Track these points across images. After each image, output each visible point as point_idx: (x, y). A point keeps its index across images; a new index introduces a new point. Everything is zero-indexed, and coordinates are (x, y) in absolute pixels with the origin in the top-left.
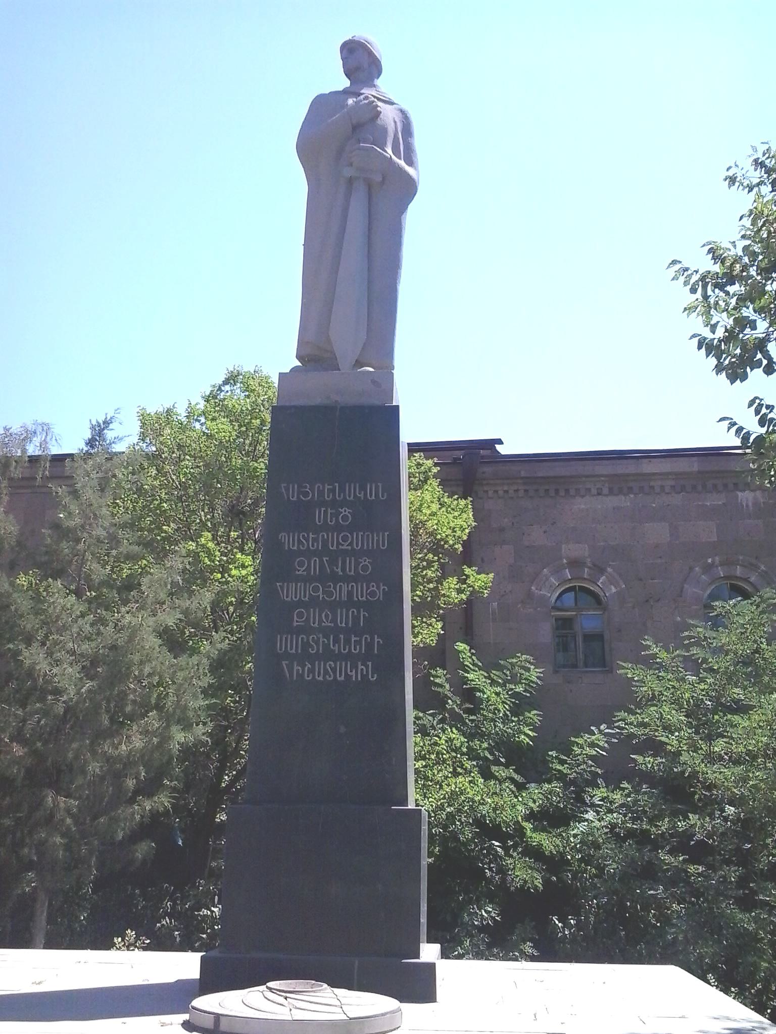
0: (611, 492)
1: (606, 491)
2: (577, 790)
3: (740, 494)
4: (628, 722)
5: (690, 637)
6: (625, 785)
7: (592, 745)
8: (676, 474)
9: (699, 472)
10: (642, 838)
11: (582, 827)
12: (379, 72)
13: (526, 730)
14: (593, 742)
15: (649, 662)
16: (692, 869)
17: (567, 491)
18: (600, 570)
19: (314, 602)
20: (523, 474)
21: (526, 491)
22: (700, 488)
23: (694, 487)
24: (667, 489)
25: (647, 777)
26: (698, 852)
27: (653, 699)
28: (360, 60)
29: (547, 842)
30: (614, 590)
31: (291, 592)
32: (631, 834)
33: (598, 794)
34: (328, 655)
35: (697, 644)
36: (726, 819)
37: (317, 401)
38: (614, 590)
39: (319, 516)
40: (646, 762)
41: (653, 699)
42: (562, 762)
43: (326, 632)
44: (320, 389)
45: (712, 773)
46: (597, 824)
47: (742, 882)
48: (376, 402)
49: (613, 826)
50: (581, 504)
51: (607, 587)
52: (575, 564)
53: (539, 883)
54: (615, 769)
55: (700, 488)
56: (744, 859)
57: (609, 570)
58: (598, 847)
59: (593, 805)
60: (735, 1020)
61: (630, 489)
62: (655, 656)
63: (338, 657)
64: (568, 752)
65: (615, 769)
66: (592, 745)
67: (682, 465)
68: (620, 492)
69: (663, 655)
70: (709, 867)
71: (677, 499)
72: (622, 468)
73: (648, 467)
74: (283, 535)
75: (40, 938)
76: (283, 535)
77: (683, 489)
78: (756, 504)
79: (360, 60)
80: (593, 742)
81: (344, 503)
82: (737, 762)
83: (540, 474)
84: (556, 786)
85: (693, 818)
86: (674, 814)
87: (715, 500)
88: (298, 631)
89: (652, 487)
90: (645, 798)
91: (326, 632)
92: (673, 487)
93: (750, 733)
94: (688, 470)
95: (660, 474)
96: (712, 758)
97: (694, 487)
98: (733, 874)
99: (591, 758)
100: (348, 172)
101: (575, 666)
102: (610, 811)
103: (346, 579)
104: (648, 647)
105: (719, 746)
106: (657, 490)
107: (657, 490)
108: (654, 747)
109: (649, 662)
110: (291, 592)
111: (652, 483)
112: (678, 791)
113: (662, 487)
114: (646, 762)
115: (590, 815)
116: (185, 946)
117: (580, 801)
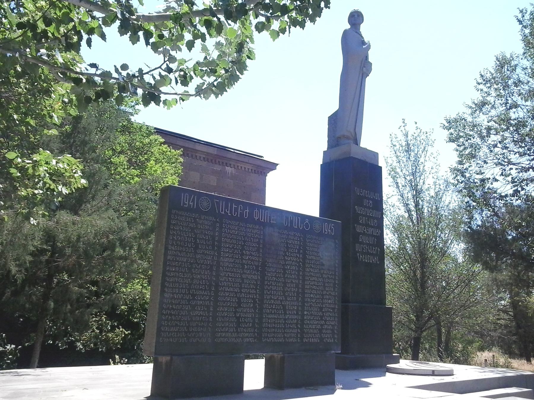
3: (227, 168)
8: (207, 153)
9: (215, 155)
22: (213, 161)
24: (202, 159)
44: (338, 153)
48: (372, 162)
55: (213, 161)
60: (355, 93)
67: (211, 150)
71: (204, 164)
72: (190, 145)
73: (198, 147)
75: (36, 360)
78: (232, 173)
87: (217, 168)
89: (196, 156)
94: (213, 153)
95: (202, 151)
106: (198, 158)
111: (197, 154)
116: (130, 354)
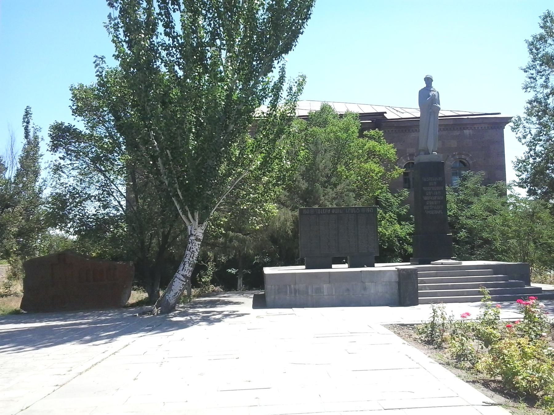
17: (409, 130)
24: (442, 130)
28: (428, 80)
34: (434, 209)
77: (447, 129)
79: (428, 80)
87: (456, 133)
100: (431, 110)
110: (426, 198)
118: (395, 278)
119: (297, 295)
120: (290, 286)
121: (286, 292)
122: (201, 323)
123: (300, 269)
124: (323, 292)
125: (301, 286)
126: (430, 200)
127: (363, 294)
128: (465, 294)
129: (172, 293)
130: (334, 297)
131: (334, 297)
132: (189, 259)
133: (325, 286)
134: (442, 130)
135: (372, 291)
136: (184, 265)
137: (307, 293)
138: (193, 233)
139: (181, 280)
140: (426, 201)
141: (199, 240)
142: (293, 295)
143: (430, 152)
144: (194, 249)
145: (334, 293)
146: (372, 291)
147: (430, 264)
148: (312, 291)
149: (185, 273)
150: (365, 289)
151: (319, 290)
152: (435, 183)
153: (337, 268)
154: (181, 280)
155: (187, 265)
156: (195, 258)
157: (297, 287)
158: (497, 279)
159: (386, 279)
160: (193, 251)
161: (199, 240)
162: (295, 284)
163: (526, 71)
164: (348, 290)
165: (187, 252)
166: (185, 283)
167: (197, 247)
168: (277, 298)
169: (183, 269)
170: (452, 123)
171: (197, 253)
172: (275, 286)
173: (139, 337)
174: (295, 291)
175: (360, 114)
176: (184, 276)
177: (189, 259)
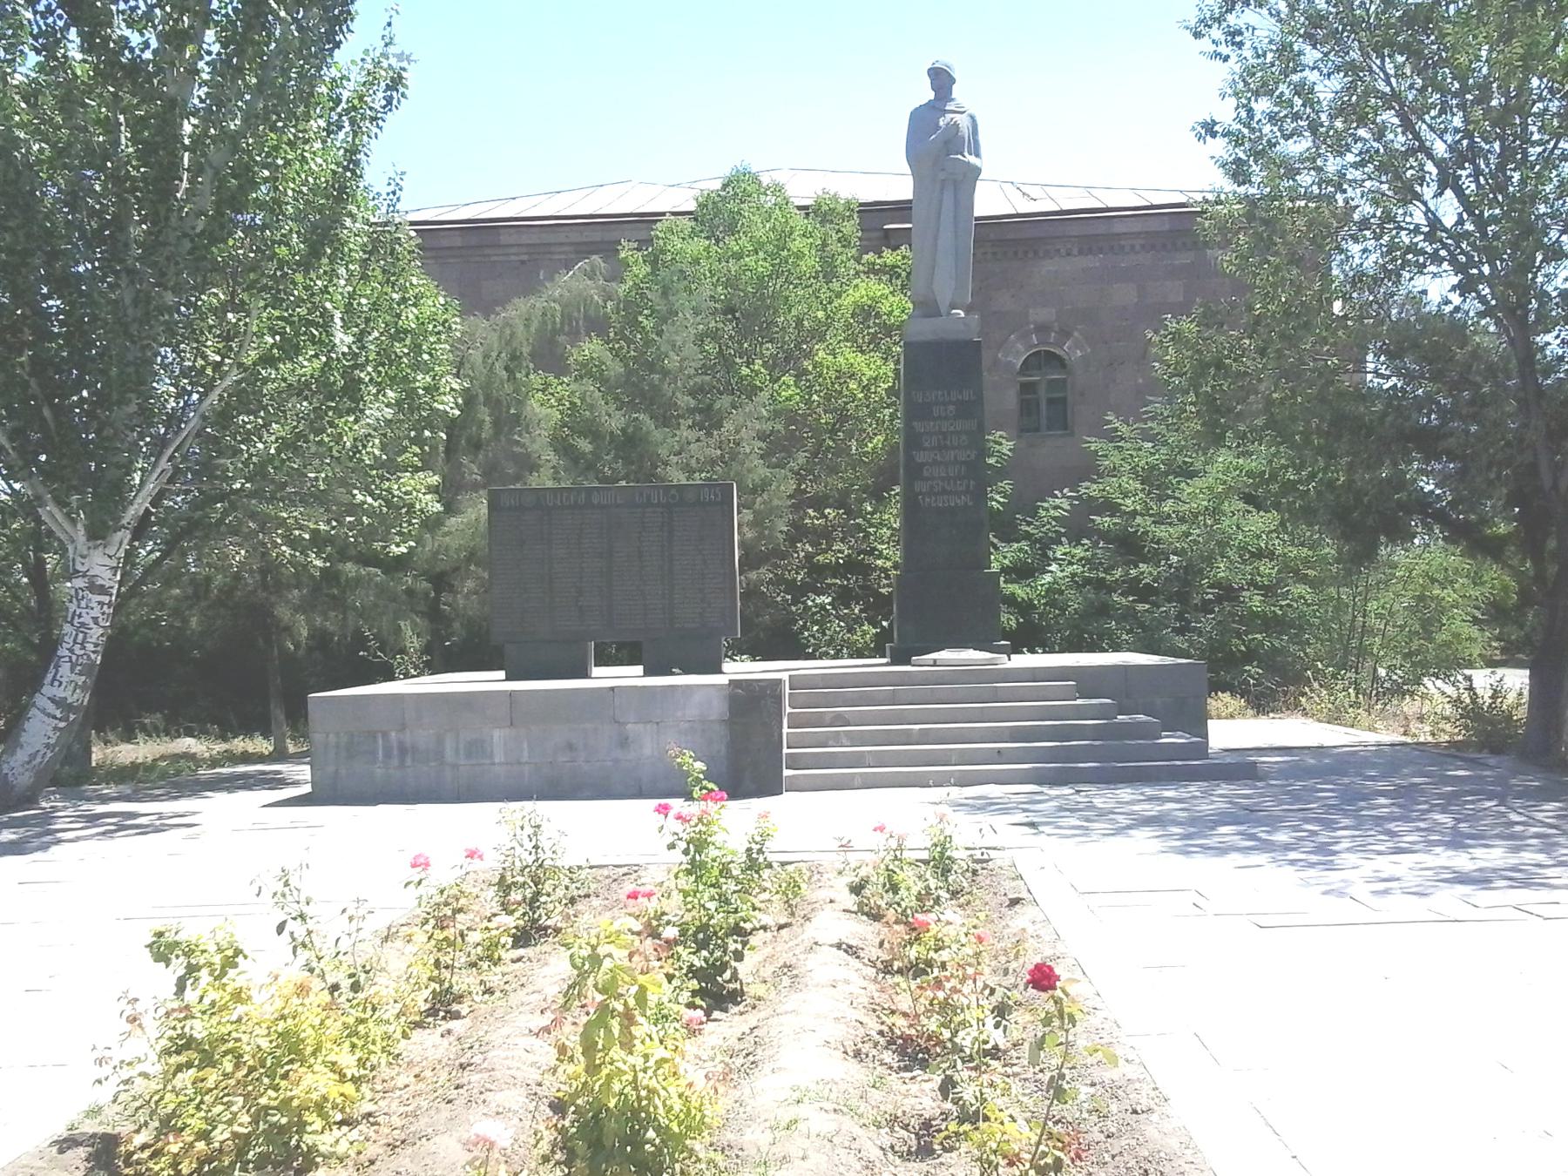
0: (1081, 252)
1: (1075, 251)
2: (1043, 547)
4: (1091, 489)
5: (1146, 412)
6: (1085, 541)
7: (1056, 508)
10: (1100, 584)
11: (1048, 578)
12: (953, 81)
13: (997, 497)
14: (1059, 504)
15: (1112, 436)
16: (1140, 607)
17: (1036, 253)
18: (1065, 334)
19: (935, 463)
20: (992, 236)
21: (994, 254)
23: (1164, 246)
24: (1138, 248)
25: (1105, 535)
26: (1144, 593)
27: (1114, 472)
28: (941, 79)
29: (1019, 591)
30: (1079, 353)
31: (920, 457)
32: (1088, 581)
33: (1059, 552)
34: (944, 492)
35: (1153, 419)
36: (1170, 566)
37: (930, 337)
38: (1079, 353)
39: (936, 411)
40: (1105, 522)
41: (1114, 472)
42: (1029, 524)
43: (943, 479)
45: (1161, 532)
46: (1060, 574)
47: (1180, 617)
49: (1074, 575)
50: (1048, 266)
51: (1072, 351)
52: (1042, 329)
53: (1013, 624)
54: (1076, 528)
56: (1182, 598)
57: (1076, 334)
58: (1061, 592)
59: (1055, 559)
61: (1101, 250)
62: (1116, 430)
63: (950, 493)
64: (1034, 514)
65: (1076, 528)
66: (1056, 508)
67: (1154, 226)
68: (1090, 251)
69: (1124, 429)
70: (1154, 604)
73: (1119, 228)
74: (915, 424)
76: (915, 424)
77: (1153, 247)
79: (941, 79)
80: (1059, 504)
81: (950, 402)
82: (1182, 520)
83: (1009, 237)
84: (1024, 544)
85: (1143, 567)
86: (1127, 563)
87: (1184, 258)
88: (927, 479)
89: (1122, 247)
90: (1102, 550)
91: (943, 479)
92: (1143, 246)
93: (1193, 495)
96: (1161, 519)
97: (1164, 246)
98: (1171, 608)
99: (1054, 518)
100: (942, 176)
101: (1037, 430)
102: (1071, 563)
103: (954, 448)
104: (1110, 422)
105: (1167, 507)
106: (1127, 249)
107: (1127, 249)
108: (1111, 508)
109: (1112, 436)
110: (920, 457)
112: (1130, 546)
113: (1133, 247)
114: (1105, 522)
115: (1054, 567)
117: (1046, 560)
118: (719, 709)
119: (409, 762)
120: (385, 735)
121: (374, 753)
122: (1438, 850)
123: (490, 681)
124: (491, 756)
125: (422, 737)
126: (935, 463)
127: (616, 761)
128: (869, 760)
129: (21, 756)
130: (526, 768)
131: (526, 768)
132: (71, 650)
133: (497, 734)
134: (1138, 248)
135: (647, 751)
136: (57, 667)
137: (439, 755)
138: (79, 567)
139: (49, 715)
140: (923, 465)
141: (103, 590)
142: (395, 762)
143: (943, 310)
144: (86, 619)
145: (525, 758)
146: (647, 751)
147: (908, 662)
148: (457, 751)
149: (60, 693)
150: (624, 742)
151: (477, 748)
152: (951, 408)
153: (605, 677)
154: (49, 715)
155: (65, 669)
156: (90, 647)
157: (408, 738)
158: (1080, 713)
159: (692, 712)
160: (83, 625)
161: (103, 590)
162: (403, 728)
163: (1197, 35)
164: (570, 747)
165: (67, 628)
166: (62, 725)
167: (96, 612)
168: (343, 772)
169: (54, 679)
170: (1167, 227)
171: (96, 633)
172: (337, 734)
173: (1462, 879)
174: (403, 750)
175: (861, 205)
176: (59, 703)
177: (71, 650)
